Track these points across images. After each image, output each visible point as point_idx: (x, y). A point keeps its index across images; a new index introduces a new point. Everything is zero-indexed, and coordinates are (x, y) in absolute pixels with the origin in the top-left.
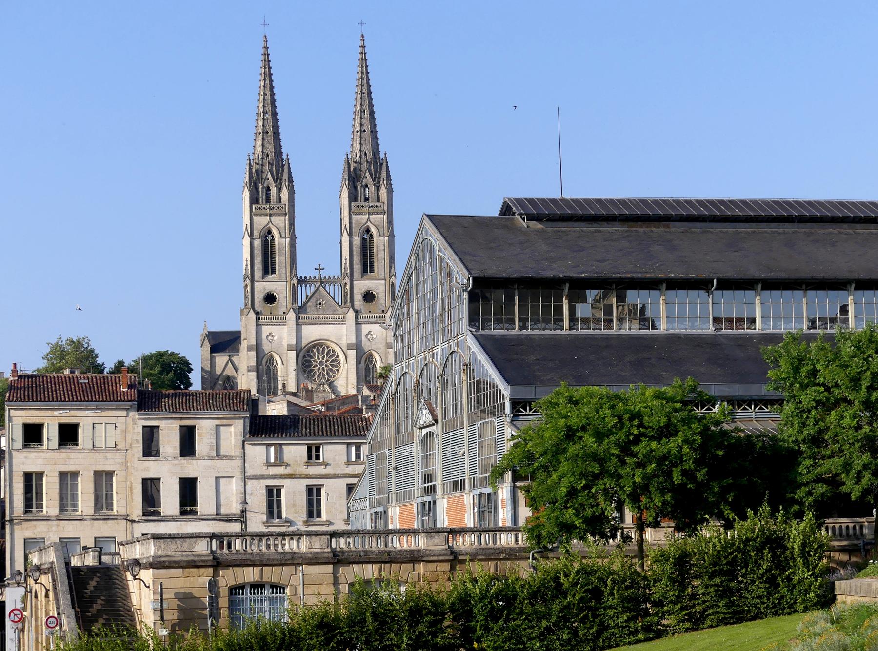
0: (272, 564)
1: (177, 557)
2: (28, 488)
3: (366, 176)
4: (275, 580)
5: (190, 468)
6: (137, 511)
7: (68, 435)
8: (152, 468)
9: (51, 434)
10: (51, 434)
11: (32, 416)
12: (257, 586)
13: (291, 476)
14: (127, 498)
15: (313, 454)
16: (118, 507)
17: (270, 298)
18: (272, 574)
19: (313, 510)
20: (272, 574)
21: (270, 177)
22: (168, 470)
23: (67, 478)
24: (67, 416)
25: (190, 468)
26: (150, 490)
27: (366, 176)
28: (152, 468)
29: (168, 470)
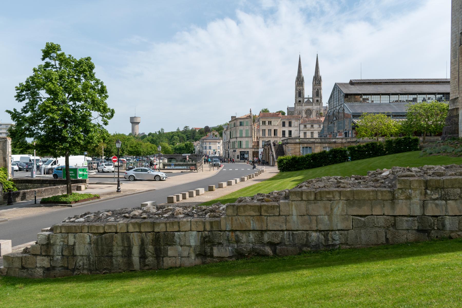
0: (309, 143)
1: (293, 142)
2: (263, 132)
3: (317, 80)
4: (310, 146)
5: (291, 129)
6: (281, 136)
7: (270, 123)
8: (284, 129)
9: (267, 123)
10: (267, 123)
11: (264, 120)
12: (307, 147)
13: (308, 130)
14: (280, 134)
15: (312, 126)
16: (278, 136)
17: (300, 101)
18: (309, 145)
19: (178, 200)
20: (309, 145)
21: (300, 81)
22: (287, 129)
23: (270, 130)
24: (269, 120)
25: (291, 129)
26: (284, 132)
27: (317, 80)
28: (284, 129)
29: (287, 129)
